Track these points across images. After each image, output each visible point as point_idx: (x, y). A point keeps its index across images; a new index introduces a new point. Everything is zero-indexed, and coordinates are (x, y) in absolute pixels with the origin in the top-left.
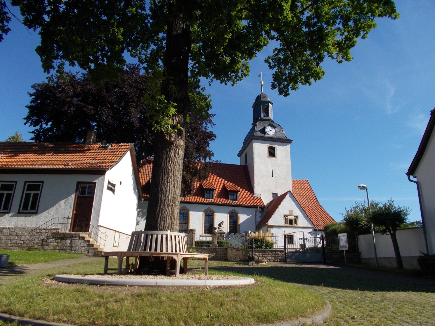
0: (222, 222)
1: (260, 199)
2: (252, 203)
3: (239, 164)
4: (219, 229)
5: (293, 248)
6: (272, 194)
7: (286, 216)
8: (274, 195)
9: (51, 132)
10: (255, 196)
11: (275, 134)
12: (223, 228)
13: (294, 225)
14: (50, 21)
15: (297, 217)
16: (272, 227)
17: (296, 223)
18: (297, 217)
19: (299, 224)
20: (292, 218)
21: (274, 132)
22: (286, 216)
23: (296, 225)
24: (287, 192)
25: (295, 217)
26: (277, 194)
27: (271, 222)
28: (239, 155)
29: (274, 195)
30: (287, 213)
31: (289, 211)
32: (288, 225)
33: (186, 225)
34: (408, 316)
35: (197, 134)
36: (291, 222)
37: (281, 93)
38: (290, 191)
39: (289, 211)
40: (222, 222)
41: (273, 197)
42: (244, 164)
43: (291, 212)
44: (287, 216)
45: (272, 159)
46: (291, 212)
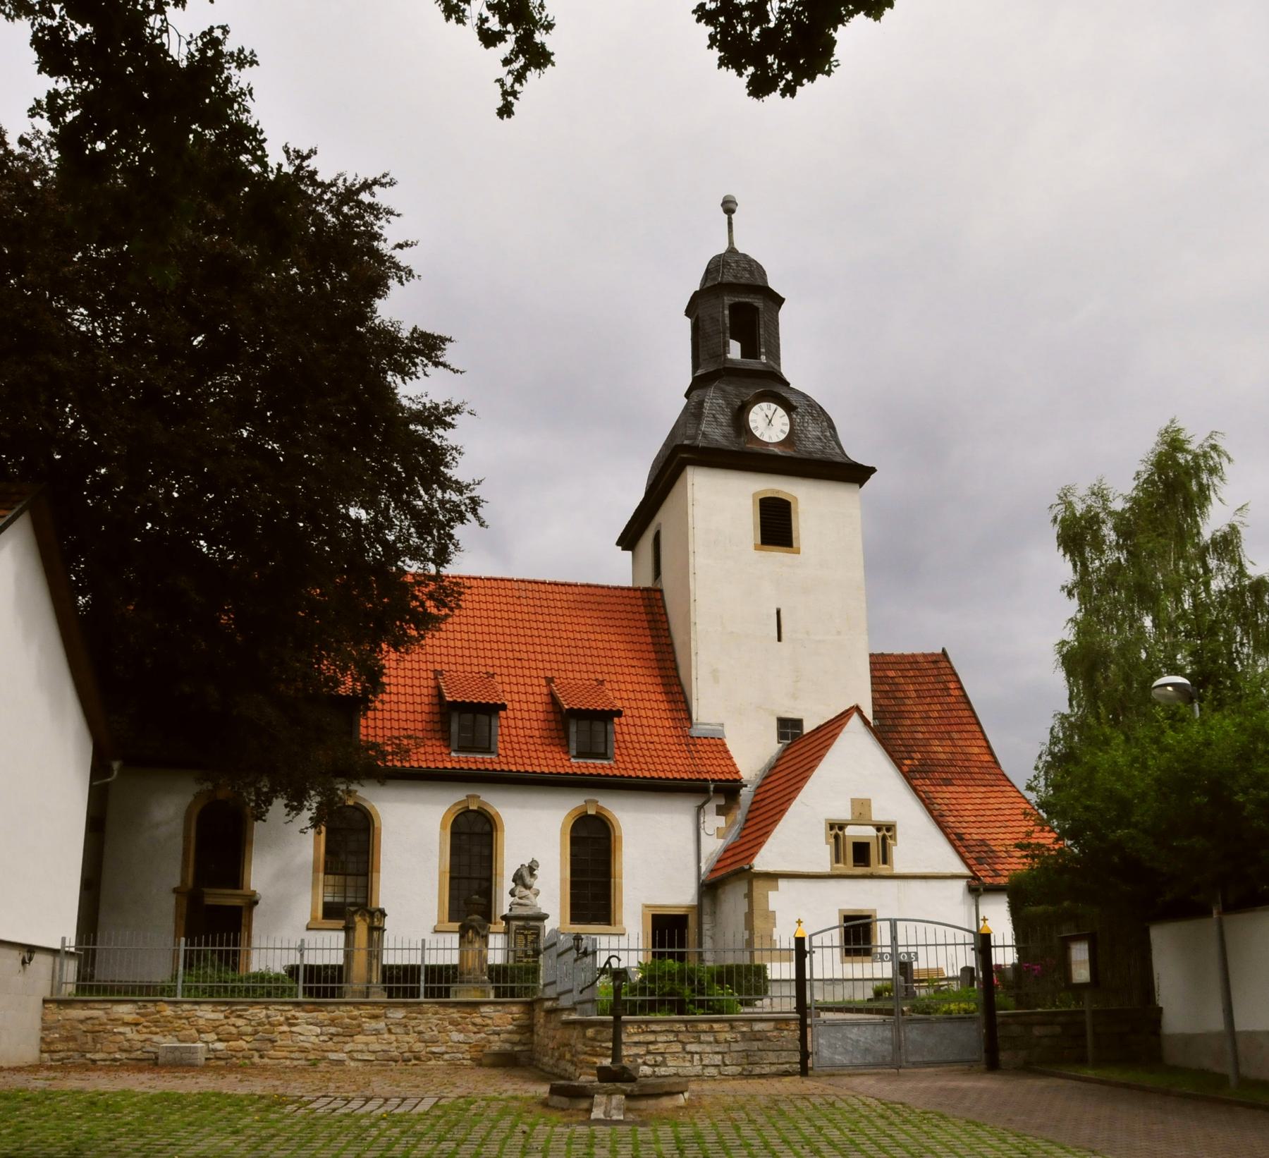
0: (532, 869)
1: (717, 745)
2: (679, 769)
3: (628, 583)
4: (516, 900)
5: (858, 975)
6: (774, 724)
7: (836, 828)
8: (788, 728)
9: (209, 548)
10: (694, 733)
11: (789, 440)
12: (537, 894)
13: (876, 867)
14: (803, 79)
15: (887, 830)
16: (773, 877)
17: (885, 859)
18: (887, 830)
19: (902, 859)
20: (868, 833)
21: (787, 429)
22: (836, 828)
23: (883, 869)
24: (843, 717)
25: (879, 829)
26: (798, 723)
27: (764, 861)
28: (628, 540)
29: (788, 728)
30: (844, 814)
31: (853, 801)
32: (847, 867)
33: (361, 880)
34: (426, 1037)
35: (1220, 606)
36: (861, 852)
37: (30, 110)
38: (857, 709)
39: (853, 801)
40: (532, 869)
41: (782, 736)
42: (647, 582)
43: (861, 809)
44: (842, 827)
45: (777, 556)
46: (861, 809)
